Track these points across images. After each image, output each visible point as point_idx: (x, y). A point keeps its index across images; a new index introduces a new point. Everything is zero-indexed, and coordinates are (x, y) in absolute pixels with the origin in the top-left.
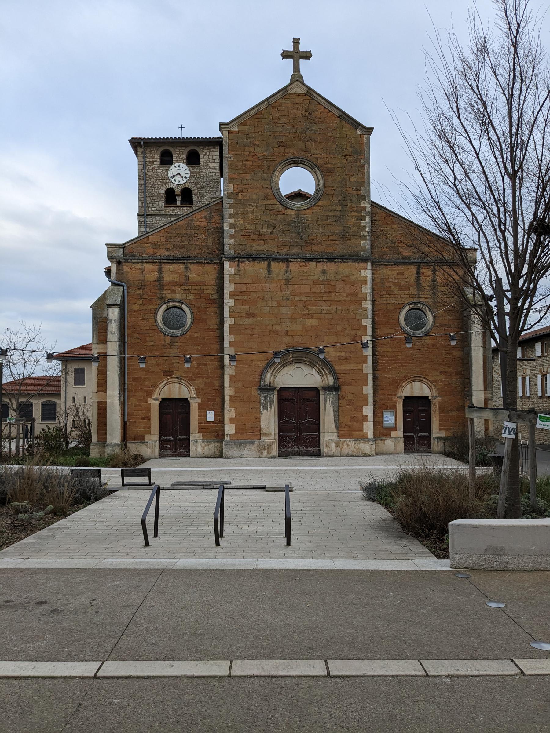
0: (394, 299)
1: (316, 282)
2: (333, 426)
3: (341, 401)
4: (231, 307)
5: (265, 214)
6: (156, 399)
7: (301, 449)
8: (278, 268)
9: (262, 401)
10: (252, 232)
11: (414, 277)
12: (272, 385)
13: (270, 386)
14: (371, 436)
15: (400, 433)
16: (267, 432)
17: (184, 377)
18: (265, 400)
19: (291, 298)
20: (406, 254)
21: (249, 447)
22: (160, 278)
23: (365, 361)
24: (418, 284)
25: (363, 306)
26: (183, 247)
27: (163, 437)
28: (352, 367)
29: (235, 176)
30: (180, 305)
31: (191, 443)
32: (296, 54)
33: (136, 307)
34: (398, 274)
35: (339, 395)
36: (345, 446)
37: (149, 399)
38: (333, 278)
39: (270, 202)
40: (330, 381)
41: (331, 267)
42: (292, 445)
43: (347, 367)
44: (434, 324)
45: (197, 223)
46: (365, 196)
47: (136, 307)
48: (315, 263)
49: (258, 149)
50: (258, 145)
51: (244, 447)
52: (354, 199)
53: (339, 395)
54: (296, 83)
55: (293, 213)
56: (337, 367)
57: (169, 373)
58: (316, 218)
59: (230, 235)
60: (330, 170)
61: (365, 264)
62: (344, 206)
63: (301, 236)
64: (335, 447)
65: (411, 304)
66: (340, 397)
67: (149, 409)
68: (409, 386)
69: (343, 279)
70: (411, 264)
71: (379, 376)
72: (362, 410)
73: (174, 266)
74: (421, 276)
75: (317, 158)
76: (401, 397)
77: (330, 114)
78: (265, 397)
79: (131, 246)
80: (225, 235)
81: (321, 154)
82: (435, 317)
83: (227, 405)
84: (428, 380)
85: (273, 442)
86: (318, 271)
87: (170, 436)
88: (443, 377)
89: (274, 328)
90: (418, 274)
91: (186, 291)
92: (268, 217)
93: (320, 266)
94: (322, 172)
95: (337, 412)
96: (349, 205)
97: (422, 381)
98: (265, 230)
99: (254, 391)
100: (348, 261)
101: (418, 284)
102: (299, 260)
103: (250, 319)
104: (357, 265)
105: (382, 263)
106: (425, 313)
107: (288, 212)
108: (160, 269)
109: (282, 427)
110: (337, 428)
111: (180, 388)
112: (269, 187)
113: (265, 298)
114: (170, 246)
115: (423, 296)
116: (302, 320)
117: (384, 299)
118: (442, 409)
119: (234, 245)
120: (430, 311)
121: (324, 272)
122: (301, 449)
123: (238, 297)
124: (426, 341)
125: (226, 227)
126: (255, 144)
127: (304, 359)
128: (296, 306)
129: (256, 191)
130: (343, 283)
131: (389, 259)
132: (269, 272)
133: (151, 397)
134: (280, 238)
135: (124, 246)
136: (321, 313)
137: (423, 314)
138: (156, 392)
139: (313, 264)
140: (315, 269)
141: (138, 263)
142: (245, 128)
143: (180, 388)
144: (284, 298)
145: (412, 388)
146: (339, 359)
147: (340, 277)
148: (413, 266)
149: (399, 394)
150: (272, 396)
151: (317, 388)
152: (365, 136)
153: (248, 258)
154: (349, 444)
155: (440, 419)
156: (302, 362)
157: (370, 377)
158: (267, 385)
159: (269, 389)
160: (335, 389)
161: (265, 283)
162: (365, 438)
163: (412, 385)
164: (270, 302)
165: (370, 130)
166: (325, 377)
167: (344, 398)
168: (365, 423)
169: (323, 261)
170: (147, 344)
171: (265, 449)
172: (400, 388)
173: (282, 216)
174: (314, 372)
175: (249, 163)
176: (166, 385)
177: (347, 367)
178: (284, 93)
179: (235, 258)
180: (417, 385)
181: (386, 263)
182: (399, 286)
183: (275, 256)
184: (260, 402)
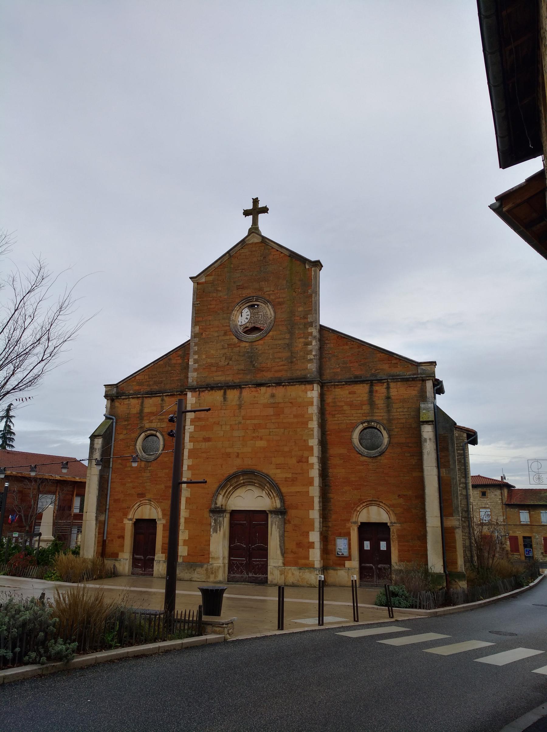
0: (346, 418)
1: (265, 406)
2: (279, 552)
3: (287, 526)
4: (191, 433)
5: (223, 348)
6: (131, 520)
7: (250, 575)
8: (232, 395)
9: (213, 524)
10: (212, 365)
11: (367, 395)
12: (224, 507)
13: (222, 508)
14: (318, 564)
15: (354, 564)
16: (215, 556)
17: (153, 499)
18: (215, 523)
19: (243, 421)
20: (358, 373)
21: (199, 570)
22: (141, 411)
23: (311, 483)
24: (371, 403)
25: (309, 426)
26: (161, 382)
27: (136, 556)
28: (298, 489)
29: (200, 319)
30: (155, 433)
31: (155, 563)
32: (256, 211)
33: (121, 437)
34: (350, 393)
35: (285, 519)
36: (290, 575)
37: (124, 519)
38: (281, 401)
39: (228, 337)
40: (278, 504)
41: (280, 391)
42: (241, 570)
43: (294, 489)
44: (390, 442)
45: (174, 361)
46: (312, 322)
47: (121, 437)
48: (265, 388)
49: (220, 294)
50: (220, 291)
51: (194, 570)
52: (301, 326)
53: (285, 519)
54: (252, 235)
55: (247, 344)
56: (284, 490)
57: (141, 495)
58: (267, 348)
59: (194, 369)
60: (280, 304)
61: (311, 386)
62: (291, 333)
63: (254, 365)
64: (279, 575)
65: (364, 423)
66: (286, 521)
67: (123, 529)
68: (365, 511)
69: (290, 401)
70: (363, 382)
71: (332, 500)
72: (308, 536)
73: (154, 399)
74: (374, 394)
75: (269, 295)
76: (355, 523)
77: (282, 255)
78: (215, 520)
79: (122, 385)
80: (189, 370)
81: (273, 291)
82: (390, 436)
83: (182, 527)
84: (384, 504)
85: (220, 566)
86: (268, 395)
87: (140, 555)
88: (401, 501)
89: (227, 451)
90: (371, 392)
91: (161, 420)
92: (226, 351)
93: (270, 390)
94: (274, 306)
95: (282, 537)
96: (297, 332)
97: (379, 506)
98: (223, 363)
99: (207, 514)
100: (295, 383)
101: (371, 403)
102: (250, 386)
103: (207, 443)
104: (303, 387)
105: (332, 383)
106: (381, 432)
107: (243, 344)
108: (142, 403)
109: (233, 551)
110: (283, 554)
111: (150, 509)
112: (228, 324)
113: (220, 423)
114: (151, 383)
115: (377, 414)
116: (251, 442)
117: (336, 419)
118: (401, 538)
119: (197, 377)
120: (384, 429)
121: (273, 396)
122: (250, 575)
123: (197, 424)
124: (381, 461)
125: (191, 363)
126: (217, 290)
127: (254, 481)
128: (247, 429)
129: (217, 329)
130: (290, 405)
131: (341, 379)
132: (225, 399)
133: (126, 518)
134: (235, 368)
135: (116, 385)
136: (270, 435)
137: (379, 433)
138: (131, 513)
139: (263, 389)
140: (264, 393)
141: (126, 399)
142: (211, 278)
143: (150, 509)
144: (237, 422)
145: (368, 513)
146: (286, 481)
147: (287, 400)
148: (365, 385)
149: (354, 520)
150: (221, 519)
151: (265, 511)
152: (313, 269)
153: (207, 388)
154: (294, 572)
155: (399, 549)
156: (252, 484)
157: (317, 500)
158: (218, 508)
159: (218, 511)
160: (281, 512)
161: (221, 410)
162: (310, 567)
163: (368, 510)
164: (224, 427)
165: (318, 264)
166: (273, 500)
167: (289, 522)
168: (311, 550)
169: (272, 386)
170: (126, 469)
171: (212, 573)
172: (355, 513)
173: (238, 349)
174: (264, 494)
175: (212, 306)
176: (139, 506)
177: (294, 489)
178: (242, 245)
179: (196, 388)
180: (374, 509)
181: (337, 383)
182: (351, 405)
183: (230, 384)
184: (210, 524)
